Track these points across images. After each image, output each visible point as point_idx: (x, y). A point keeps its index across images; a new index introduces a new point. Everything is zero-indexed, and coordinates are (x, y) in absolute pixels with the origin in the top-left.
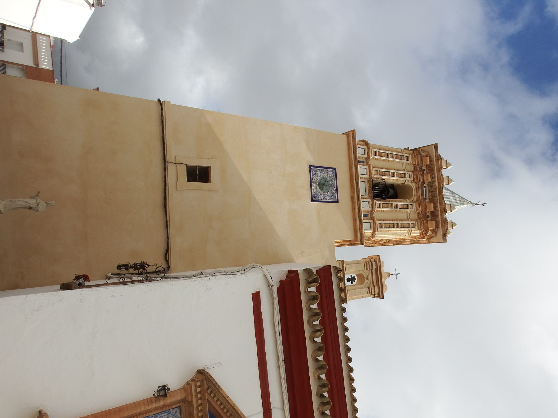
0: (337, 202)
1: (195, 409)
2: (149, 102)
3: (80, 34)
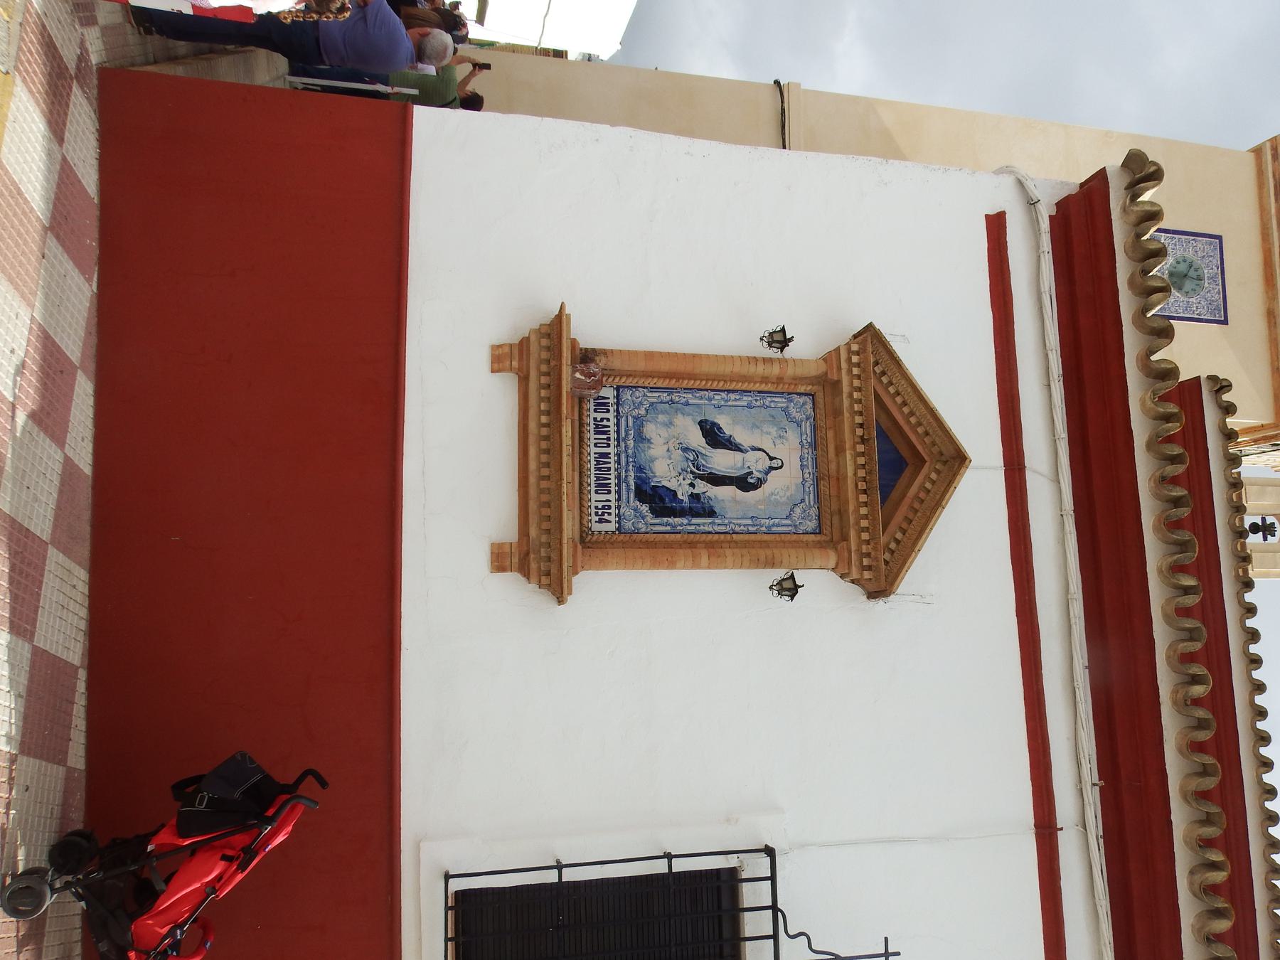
0: (1225, 322)
1: (845, 396)
2: (756, 87)
3: (623, 34)
